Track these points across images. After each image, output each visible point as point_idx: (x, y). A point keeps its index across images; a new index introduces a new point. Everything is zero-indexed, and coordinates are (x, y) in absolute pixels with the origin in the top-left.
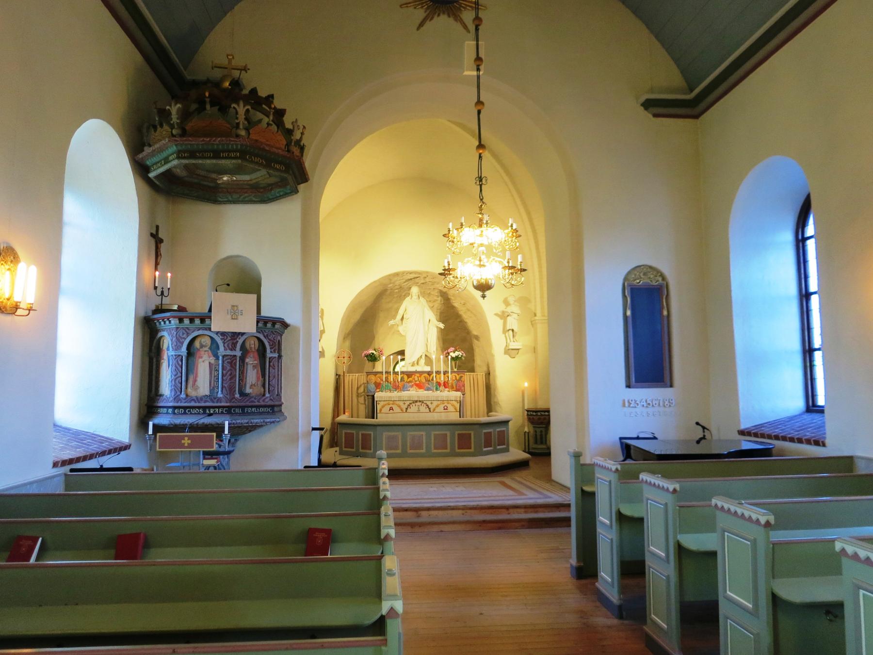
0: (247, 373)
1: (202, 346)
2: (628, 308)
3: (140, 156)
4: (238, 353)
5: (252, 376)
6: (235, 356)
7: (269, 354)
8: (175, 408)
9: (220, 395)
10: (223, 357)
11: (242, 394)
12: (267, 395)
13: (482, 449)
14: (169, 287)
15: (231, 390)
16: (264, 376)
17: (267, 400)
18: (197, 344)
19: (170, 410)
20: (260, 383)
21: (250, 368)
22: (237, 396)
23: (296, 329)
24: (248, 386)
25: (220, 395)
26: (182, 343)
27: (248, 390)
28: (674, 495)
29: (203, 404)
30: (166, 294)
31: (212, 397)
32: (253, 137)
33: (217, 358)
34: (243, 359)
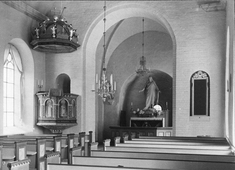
0: (85, 109)
1: (49, 103)
2: (82, 96)
3: (31, 43)
4: (59, 105)
5: (63, 111)
6: (57, 106)
7: (69, 105)
8: (42, 120)
9: (53, 117)
10: (54, 106)
11: (60, 117)
12: (68, 117)
13: (130, 127)
14: (42, 85)
15: (57, 116)
16: (67, 111)
17: (68, 119)
18: (48, 102)
19: (41, 121)
20: (66, 113)
21: (63, 109)
22: (59, 117)
23: (81, 97)
24: (62, 114)
25: (53, 117)
26: (44, 102)
27: (62, 116)
28: (179, 38)
29: (49, 119)
30: (41, 87)
31: (51, 117)
32: (58, 37)
33: (53, 106)
34: (60, 106)
